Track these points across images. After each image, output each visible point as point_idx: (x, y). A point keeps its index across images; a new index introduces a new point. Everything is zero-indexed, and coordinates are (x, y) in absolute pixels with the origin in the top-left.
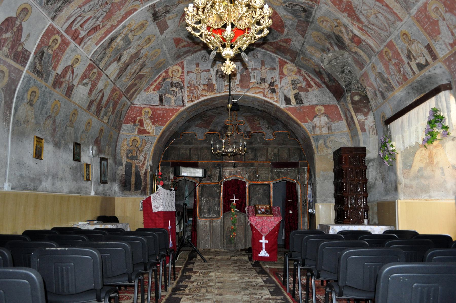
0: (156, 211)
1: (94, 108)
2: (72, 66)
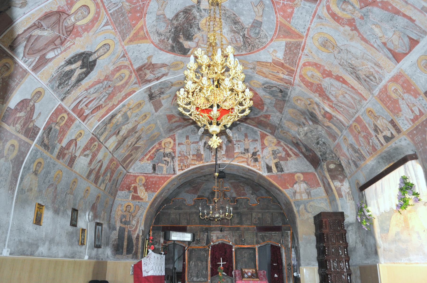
0: (146, 276)
1: (93, 177)
2: (75, 140)
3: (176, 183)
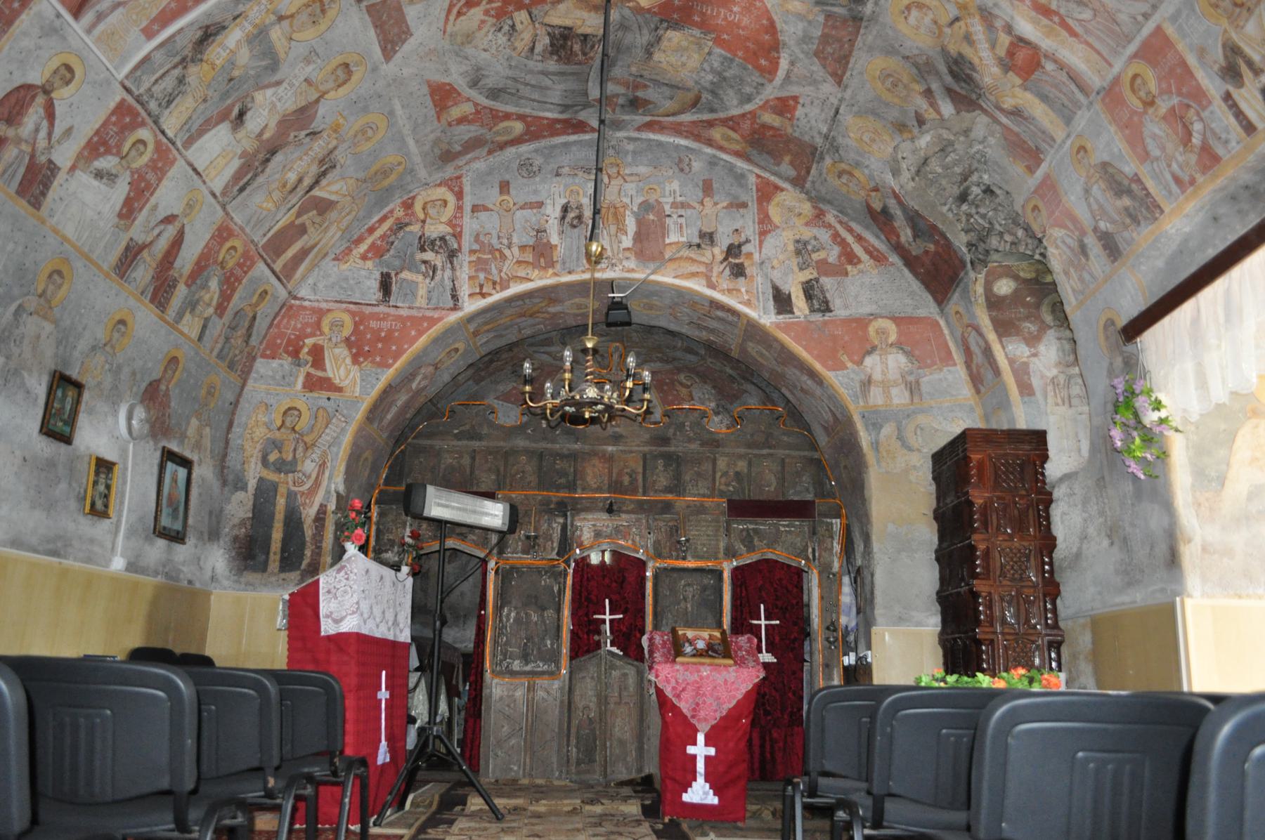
0: (332, 632)
1: (143, 273)
2: (46, 90)
3: (461, 346)
